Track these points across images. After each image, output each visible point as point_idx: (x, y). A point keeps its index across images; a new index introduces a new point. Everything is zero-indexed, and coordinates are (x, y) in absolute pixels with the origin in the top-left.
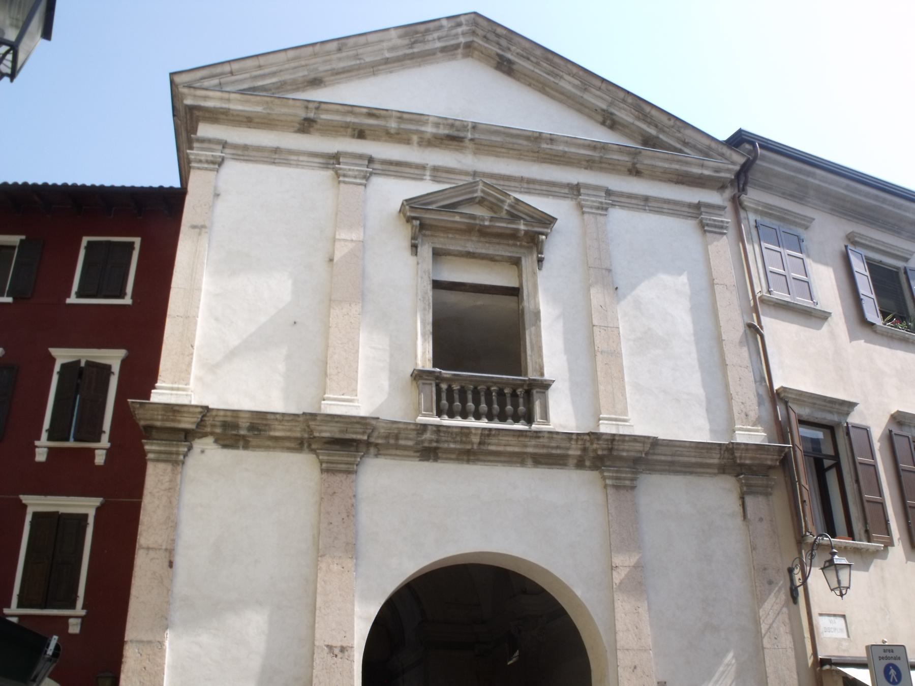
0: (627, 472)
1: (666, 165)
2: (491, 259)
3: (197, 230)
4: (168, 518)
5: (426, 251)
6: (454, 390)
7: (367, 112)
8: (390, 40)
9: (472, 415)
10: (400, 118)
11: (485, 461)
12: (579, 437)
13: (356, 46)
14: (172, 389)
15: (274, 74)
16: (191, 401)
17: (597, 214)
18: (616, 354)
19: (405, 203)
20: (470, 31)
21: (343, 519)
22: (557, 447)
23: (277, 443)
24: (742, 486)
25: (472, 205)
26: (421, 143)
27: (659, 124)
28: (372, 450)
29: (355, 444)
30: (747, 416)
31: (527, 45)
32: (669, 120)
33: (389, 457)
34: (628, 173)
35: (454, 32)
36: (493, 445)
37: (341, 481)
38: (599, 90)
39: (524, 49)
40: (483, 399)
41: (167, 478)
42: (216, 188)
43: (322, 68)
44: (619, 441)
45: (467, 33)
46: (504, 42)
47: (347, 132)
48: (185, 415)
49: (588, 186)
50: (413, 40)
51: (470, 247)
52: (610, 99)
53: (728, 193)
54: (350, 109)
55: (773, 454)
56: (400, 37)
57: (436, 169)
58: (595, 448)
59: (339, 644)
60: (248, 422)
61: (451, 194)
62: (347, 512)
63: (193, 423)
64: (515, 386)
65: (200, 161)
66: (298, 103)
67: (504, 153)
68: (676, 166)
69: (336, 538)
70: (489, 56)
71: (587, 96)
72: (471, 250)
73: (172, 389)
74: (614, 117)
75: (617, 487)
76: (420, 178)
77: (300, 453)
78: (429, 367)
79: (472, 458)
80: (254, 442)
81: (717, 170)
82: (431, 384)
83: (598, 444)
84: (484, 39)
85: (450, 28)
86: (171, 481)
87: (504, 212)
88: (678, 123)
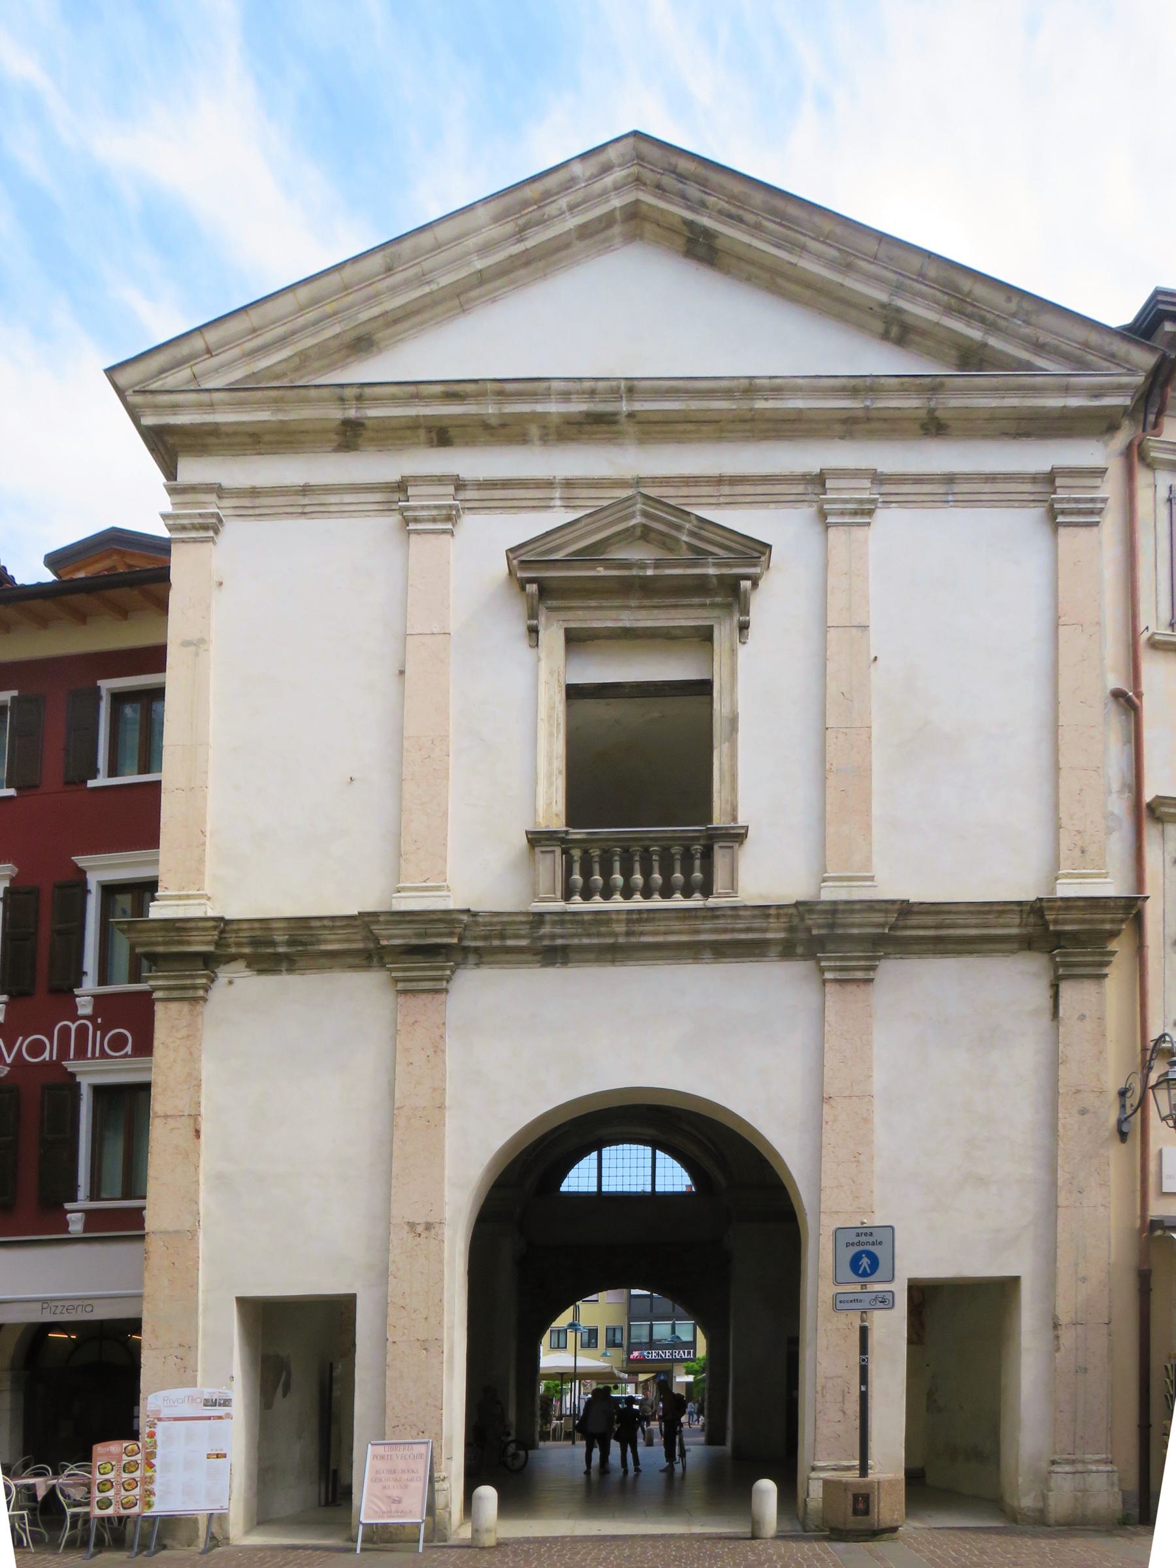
3: (192, 649)
4: (190, 1074)
5: (553, 636)
6: (592, 857)
7: (443, 393)
8: (477, 230)
12: (781, 912)
13: (417, 254)
14: (179, 897)
15: (282, 341)
16: (206, 912)
18: (864, 773)
19: (511, 556)
20: (630, 179)
25: (631, 542)
26: (546, 438)
30: (1083, 852)
31: (737, 188)
32: (1009, 300)
35: (598, 186)
39: (732, 198)
43: (364, 316)
44: (844, 911)
45: (625, 185)
46: (693, 191)
50: (521, 222)
53: (1120, 440)
54: (412, 389)
56: (497, 219)
57: (569, 484)
59: (422, 1221)
63: (208, 943)
64: (686, 843)
66: (325, 392)
70: (671, 229)
71: (853, 283)
72: (628, 624)
73: (179, 897)
74: (904, 317)
77: (368, 971)
81: (1098, 392)
82: (553, 852)
84: (657, 191)
85: (589, 179)
86: (189, 1025)
87: (684, 547)
88: (1026, 305)
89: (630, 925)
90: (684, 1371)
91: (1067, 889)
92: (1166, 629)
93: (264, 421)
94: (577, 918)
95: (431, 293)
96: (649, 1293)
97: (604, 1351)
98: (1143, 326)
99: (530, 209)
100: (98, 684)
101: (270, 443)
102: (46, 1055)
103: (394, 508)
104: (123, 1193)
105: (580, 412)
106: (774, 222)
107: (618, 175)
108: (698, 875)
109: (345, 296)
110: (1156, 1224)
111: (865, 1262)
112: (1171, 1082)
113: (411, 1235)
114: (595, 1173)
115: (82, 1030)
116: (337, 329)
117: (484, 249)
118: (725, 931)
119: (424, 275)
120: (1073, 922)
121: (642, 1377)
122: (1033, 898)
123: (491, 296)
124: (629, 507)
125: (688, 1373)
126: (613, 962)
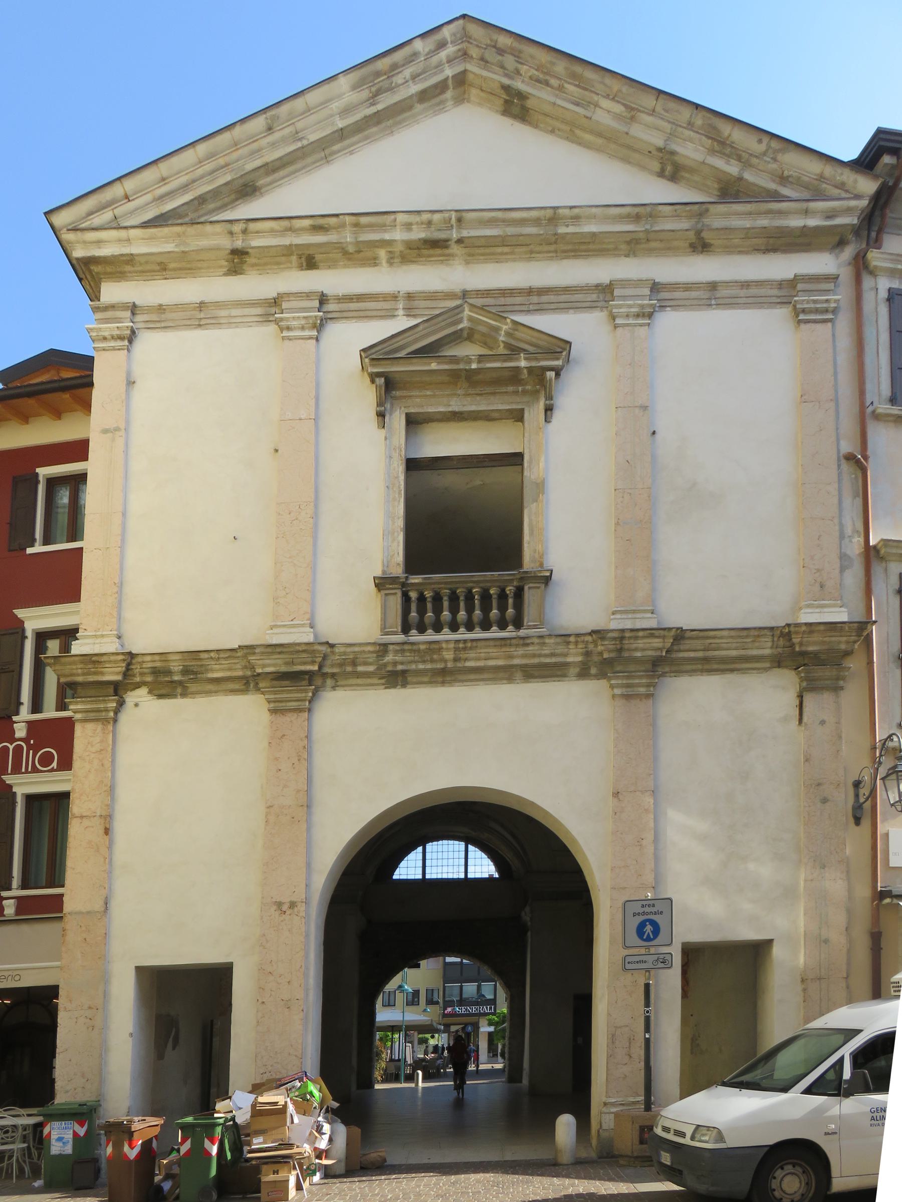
0: (640, 677)
1: (747, 224)
3: (109, 435)
5: (398, 420)
8: (340, 96)
10: (356, 225)
12: (579, 639)
17: (635, 325)
19: (363, 354)
21: (293, 764)
22: (553, 655)
24: (801, 681)
27: (744, 154)
28: (329, 682)
29: (307, 677)
32: (760, 141)
35: (435, 60)
36: (121, 660)
38: (652, 115)
40: (462, 604)
41: (98, 739)
42: (129, 374)
43: (250, 166)
44: (630, 638)
45: (455, 58)
46: (510, 61)
47: (291, 263)
48: (107, 666)
49: (625, 283)
50: (373, 89)
51: (456, 405)
52: (668, 127)
53: (848, 252)
55: (848, 634)
56: (355, 87)
57: (410, 296)
58: (600, 651)
60: (180, 666)
62: (298, 756)
63: (118, 673)
67: (506, 254)
68: (764, 222)
69: (285, 786)
71: (637, 131)
72: (457, 409)
75: (627, 697)
76: (390, 315)
77: (246, 694)
78: (397, 569)
79: (448, 679)
80: (193, 687)
81: (830, 215)
83: (602, 645)
85: (428, 53)
86: (101, 741)
87: (502, 345)
88: (774, 144)
89: (457, 652)
90: (487, 1022)
93: (169, 252)
94: (415, 647)
95: (303, 147)
97: (425, 1008)
99: (382, 79)
100: (37, 471)
101: (175, 270)
103: (270, 319)
105: (420, 240)
107: (450, 50)
108: (510, 611)
109: (234, 151)
110: (883, 895)
111: (649, 928)
114: (420, 863)
116: (228, 178)
117: (346, 111)
118: (534, 656)
120: (815, 643)
121: (453, 1028)
124: (458, 314)
125: (490, 1024)
126: (443, 683)
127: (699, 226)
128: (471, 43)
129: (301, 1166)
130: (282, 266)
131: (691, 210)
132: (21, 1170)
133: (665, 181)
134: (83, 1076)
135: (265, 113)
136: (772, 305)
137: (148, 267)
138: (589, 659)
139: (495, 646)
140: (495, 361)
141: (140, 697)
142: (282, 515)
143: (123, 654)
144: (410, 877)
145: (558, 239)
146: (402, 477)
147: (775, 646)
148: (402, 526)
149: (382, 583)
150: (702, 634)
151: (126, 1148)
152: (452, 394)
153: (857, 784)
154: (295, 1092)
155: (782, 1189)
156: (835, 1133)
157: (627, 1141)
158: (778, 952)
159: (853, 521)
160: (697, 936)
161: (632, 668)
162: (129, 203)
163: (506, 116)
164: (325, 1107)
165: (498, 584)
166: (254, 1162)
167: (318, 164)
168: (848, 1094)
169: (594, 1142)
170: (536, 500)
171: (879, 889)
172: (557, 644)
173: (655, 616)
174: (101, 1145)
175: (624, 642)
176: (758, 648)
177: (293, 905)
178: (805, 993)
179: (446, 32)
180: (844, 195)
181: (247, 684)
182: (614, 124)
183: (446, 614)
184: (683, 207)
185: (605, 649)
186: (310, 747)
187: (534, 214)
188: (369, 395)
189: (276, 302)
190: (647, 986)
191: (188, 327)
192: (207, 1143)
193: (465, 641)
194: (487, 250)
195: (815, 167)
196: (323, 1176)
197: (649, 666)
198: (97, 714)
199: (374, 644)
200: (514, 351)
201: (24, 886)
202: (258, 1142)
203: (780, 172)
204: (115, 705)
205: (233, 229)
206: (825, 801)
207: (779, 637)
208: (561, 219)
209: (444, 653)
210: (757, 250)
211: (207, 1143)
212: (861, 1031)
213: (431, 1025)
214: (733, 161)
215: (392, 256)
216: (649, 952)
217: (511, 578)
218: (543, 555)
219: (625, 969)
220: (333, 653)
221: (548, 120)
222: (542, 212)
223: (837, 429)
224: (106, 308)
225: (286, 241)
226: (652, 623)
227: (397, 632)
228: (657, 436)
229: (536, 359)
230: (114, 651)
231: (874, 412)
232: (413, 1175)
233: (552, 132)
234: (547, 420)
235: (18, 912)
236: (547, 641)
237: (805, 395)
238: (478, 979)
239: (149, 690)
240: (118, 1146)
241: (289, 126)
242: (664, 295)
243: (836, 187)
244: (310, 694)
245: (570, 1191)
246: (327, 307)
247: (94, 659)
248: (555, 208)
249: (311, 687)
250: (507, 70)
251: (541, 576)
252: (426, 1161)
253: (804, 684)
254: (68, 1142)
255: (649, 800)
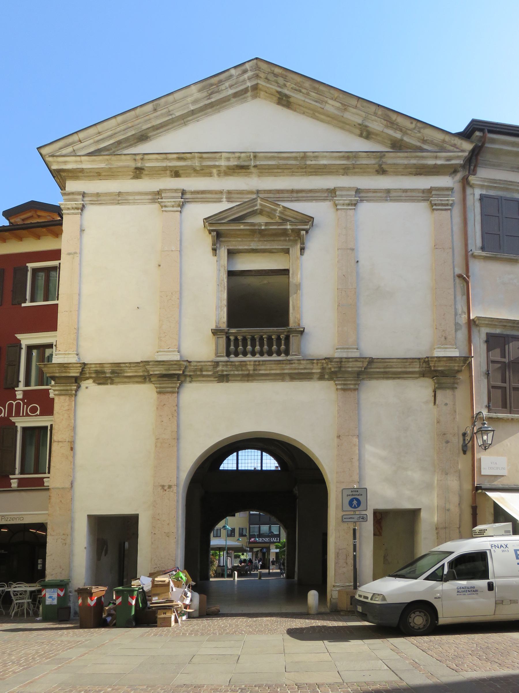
0: (351, 380)
1: (406, 162)
2: (271, 251)
5: (223, 252)
7: (177, 157)
8: (192, 95)
9: (250, 353)
10: (201, 158)
11: (258, 380)
12: (319, 362)
17: (347, 209)
20: (254, 76)
23: (131, 379)
24: (435, 384)
27: (403, 129)
28: (188, 379)
29: (176, 376)
32: (412, 123)
33: (198, 382)
34: (376, 173)
35: (242, 78)
36: (262, 370)
37: (168, 398)
40: (257, 343)
41: (67, 404)
42: (81, 226)
43: (145, 127)
44: (345, 362)
46: (281, 80)
47: (166, 174)
49: (342, 189)
50: (209, 92)
52: (363, 114)
53: (459, 176)
55: (459, 362)
56: (199, 91)
57: (229, 192)
60: (110, 369)
61: (237, 210)
63: (77, 373)
65: (68, 209)
68: (413, 161)
72: (254, 248)
75: (344, 390)
76: (219, 201)
77: (144, 384)
78: (224, 326)
80: (116, 380)
81: (449, 159)
84: (266, 80)
86: (68, 405)
87: (278, 218)
88: (419, 125)
89: (255, 366)
90: (275, 547)
91: (438, 353)
92: (479, 251)
93: (102, 168)
94: (233, 364)
95: (172, 118)
96: (258, 513)
97: (238, 538)
98: (468, 133)
99: (213, 87)
100: (27, 265)
102: (3, 415)
103: (156, 201)
104: (34, 471)
105: (234, 165)
106: (314, 92)
107: (250, 74)
108: (283, 347)
109: (137, 120)
110: (477, 488)
111: (355, 502)
112: (483, 431)
113: (162, 490)
114: (235, 462)
115: (18, 405)
116: (133, 132)
117: (195, 102)
118: (295, 369)
119: (169, 112)
120: (441, 366)
121: (255, 550)
122: (425, 357)
123: (197, 119)
124: (254, 202)
126: (248, 381)
127: (381, 162)
128: (261, 71)
129: (177, 611)
130: (161, 175)
131: (376, 155)
132: (28, 613)
133: (362, 139)
134: (60, 567)
135: (153, 102)
136: (419, 201)
137: (91, 174)
138: (324, 371)
139: (275, 364)
140: (274, 225)
141: (89, 384)
142: (162, 297)
143: (80, 363)
144: (229, 469)
145: (306, 167)
146: (226, 280)
147: (421, 367)
148: (226, 304)
149: (216, 332)
150: (383, 360)
151: (89, 600)
152: (252, 241)
153: (464, 435)
154: (173, 577)
155: (414, 623)
156: (440, 598)
157: (344, 604)
158: (423, 515)
159: (462, 307)
160: (382, 506)
161: (346, 375)
162: (82, 144)
163: (279, 105)
164: (188, 584)
165: (277, 334)
166: (154, 608)
167: (180, 126)
168: (446, 580)
169: (329, 604)
170: (296, 293)
171: (476, 485)
172: (307, 363)
173: (358, 351)
174: (70, 601)
175: (342, 363)
176: (412, 368)
177: (170, 487)
178: (437, 535)
179: (247, 66)
180: (456, 150)
181: (145, 379)
182: (336, 112)
183: (249, 348)
184: (372, 153)
185: (333, 367)
186: (178, 410)
187: (294, 155)
188: (208, 240)
189: (159, 193)
190: (354, 530)
191: (112, 204)
192: (130, 599)
193: (259, 361)
194: (270, 171)
195: (440, 136)
196: (187, 617)
197: (356, 375)
198: (66, 392)
199: (212, 361)
200: (284, 221)
201: (22, 473)
202: (155, 599)
203: (423, 138)
204: (76, 388)
205: (136, 158)
206: (447, 442)
207: (423, 363)
208: (308, 157)
209: (248, 367)
210: (411, 174)
211: (130, 599)
212: (454, 552)
213: (242, 548)
214: (398, 132)
215: (220, 172)
216: (355, 513)
217: (283, 331)
218: (300, 320)
219: (343, 521)
220: (190, 365)
221: (301, 108)
222: (298, 154)
223: (453, 262)
224: (69, 194)
225: (164, 164)
226: (357, 355)
227: (223, 356)
228: (359, 263)
229: (296, 225)
230: (75, 362)
231: (472, 254)
232: (234, 618)
233: (304, 113)
234: (302, 254)
235: (19, 486)
236: (302, 362)
237: (436, 245)
238: (270, 523)
239: (94, 381)
240: (84, 600)
241: (164, 109)
242: (362, 195)
243: (452, 146)
244: (178, 385)
245: (314, 625)
246: (185, 196)
247: (65, 365)
248: (305, 152)
249: (178, 382)
250: (279, 84)
251: (299, 331)
252: (241, 612)
253: (437, 386)
254: (55, 598)
255: (355, 440)
